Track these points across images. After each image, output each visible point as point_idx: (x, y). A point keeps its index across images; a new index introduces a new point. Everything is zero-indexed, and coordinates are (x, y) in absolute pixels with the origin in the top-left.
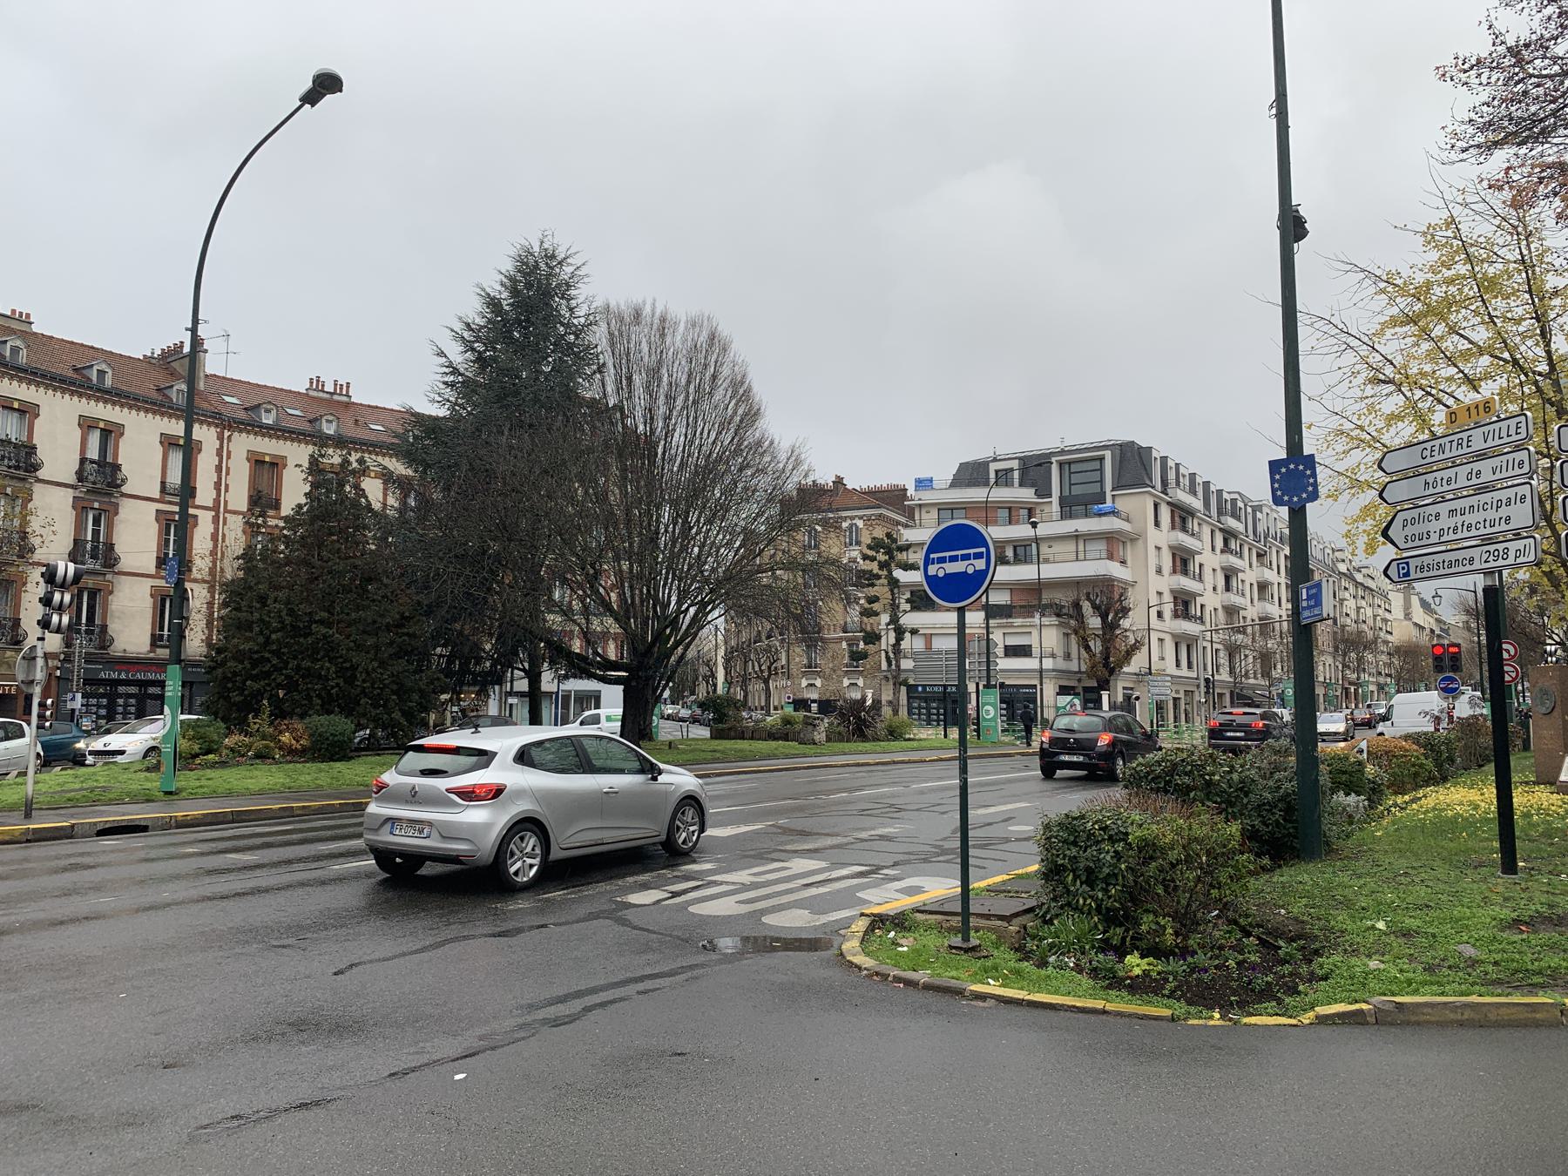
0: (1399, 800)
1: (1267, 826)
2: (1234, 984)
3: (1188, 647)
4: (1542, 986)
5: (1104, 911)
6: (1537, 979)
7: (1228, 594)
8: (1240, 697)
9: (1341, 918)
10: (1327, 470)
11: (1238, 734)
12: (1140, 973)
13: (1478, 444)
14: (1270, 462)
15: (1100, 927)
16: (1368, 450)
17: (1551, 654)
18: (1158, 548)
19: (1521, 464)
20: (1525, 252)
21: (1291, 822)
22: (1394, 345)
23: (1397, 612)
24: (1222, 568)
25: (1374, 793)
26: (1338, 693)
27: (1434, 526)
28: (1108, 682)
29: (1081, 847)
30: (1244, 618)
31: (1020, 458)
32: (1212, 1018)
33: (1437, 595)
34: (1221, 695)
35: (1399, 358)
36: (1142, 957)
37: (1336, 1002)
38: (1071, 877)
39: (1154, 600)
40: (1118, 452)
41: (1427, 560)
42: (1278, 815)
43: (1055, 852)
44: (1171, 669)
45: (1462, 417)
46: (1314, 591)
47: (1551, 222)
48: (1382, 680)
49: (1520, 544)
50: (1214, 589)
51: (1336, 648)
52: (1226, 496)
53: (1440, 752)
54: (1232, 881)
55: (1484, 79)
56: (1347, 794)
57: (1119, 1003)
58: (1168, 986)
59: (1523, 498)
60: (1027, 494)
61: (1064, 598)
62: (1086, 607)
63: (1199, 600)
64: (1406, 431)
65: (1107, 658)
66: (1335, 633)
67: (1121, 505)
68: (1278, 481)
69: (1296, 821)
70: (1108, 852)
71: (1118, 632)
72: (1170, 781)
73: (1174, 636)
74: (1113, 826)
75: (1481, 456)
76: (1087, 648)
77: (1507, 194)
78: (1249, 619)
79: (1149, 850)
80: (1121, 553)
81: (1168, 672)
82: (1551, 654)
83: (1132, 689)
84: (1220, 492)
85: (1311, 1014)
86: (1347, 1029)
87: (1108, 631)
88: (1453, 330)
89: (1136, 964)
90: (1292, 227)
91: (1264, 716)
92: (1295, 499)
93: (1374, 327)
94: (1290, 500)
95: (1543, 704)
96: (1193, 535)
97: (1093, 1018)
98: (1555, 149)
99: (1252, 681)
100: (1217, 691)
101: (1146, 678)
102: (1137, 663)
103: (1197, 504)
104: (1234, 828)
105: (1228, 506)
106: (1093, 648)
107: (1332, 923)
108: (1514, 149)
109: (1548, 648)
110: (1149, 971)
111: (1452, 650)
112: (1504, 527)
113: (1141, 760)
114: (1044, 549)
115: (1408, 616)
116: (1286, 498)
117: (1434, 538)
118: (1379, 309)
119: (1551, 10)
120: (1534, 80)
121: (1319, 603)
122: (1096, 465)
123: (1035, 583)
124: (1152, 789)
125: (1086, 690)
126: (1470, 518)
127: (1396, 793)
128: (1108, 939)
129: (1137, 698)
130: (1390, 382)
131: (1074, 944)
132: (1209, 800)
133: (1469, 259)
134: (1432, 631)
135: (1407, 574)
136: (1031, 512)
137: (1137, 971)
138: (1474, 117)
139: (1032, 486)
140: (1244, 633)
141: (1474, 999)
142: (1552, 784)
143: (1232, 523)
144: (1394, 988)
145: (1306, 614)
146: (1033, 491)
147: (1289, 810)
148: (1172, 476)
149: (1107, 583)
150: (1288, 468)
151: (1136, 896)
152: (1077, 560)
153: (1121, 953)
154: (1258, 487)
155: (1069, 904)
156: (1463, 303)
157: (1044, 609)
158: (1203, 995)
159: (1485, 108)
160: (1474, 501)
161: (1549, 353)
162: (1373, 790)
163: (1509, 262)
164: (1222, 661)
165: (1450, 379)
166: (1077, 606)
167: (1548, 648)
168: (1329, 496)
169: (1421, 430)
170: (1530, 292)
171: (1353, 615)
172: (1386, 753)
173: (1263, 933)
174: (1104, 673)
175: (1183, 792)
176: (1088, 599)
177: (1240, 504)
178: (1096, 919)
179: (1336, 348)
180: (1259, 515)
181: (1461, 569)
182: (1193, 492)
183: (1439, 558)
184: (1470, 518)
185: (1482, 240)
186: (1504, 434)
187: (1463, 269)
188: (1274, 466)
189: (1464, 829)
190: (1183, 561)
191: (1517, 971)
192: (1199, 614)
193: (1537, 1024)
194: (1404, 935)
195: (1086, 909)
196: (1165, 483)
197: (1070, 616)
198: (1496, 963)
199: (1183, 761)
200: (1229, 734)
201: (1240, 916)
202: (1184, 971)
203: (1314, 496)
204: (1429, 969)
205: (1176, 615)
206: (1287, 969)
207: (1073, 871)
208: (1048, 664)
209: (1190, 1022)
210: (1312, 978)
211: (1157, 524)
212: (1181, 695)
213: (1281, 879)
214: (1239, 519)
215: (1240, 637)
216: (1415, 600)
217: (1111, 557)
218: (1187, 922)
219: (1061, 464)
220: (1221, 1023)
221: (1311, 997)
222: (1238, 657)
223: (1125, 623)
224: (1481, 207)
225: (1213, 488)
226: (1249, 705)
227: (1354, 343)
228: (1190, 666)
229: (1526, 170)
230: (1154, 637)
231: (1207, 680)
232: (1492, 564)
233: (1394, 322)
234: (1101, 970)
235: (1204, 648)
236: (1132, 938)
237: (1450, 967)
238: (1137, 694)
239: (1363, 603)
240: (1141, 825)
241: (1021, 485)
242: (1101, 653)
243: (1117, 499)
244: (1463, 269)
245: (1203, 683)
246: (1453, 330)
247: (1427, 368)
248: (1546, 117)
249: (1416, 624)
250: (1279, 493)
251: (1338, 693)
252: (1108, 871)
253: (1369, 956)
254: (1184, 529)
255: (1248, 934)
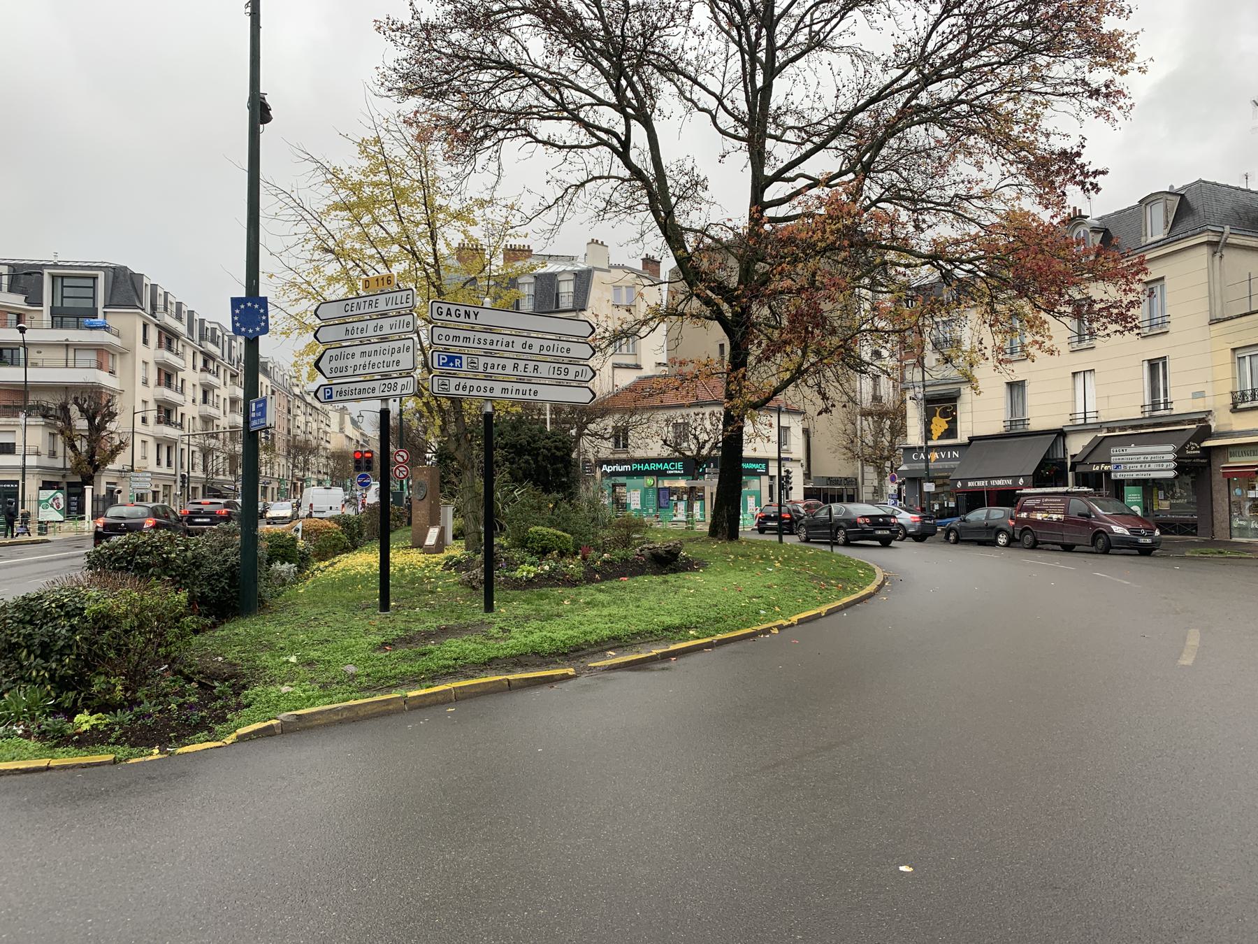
0: (322, 565)
1: (215, 592)
2: (173, 723)
3: (169, 448)
4: (395, 686)
5: (57, 679)
6: (393, 682)
7: (205, 406)
8: (211, 489)
9: (265, 658)
10: (282, 312)
11: (205, 520)
12: (88, 728)
13: (382, 306)
14: (233, 299)
15: (53, 694)
16: (313, 301)
17: (429, 460)
18: (145, 363)
19: (408, 324)
20: (424, 176)
21: (234, 587)
22: (337, 223)
23: (335, 427)
24: (201, 384)
25: (303, 561)
26: (289, 487)
27: (351, 362)
28: (92, 477)
29: (37, 625)
30: (217, 426)
31: (9, 265)
32: (151, 754)
33: (360, 416)
34: (195, 489)
35: (338, 235)
36: (91, 714)
37: (254, 722)
38: (24, 653)
39: (139, 407)
40: (111, 274)
41: (345, 387)
42: (224, 582)
43: (9, 632)
44: (153, 467)
45: (373, 284)
46: (261, 405)
47: (440, 158)
48: (321, 477)
49: (404, 381)
50: (194, 401)
51: (289, 453)
52: (207, 324)
53: (353, 529)
54: (178, 639)
55: (406, 43)
56: (282, 563)
57: (63, 758)
58: (114, 735)
59: (408, 348)
60: (17, 301)
61: (51, 401)
62: (74, 410)
63: (180, 410)
64: (340, 291)
65: (93, 456)
66: (289, 441)
67: (112, 321)
68: (237, 315)
69: (238, 586)
70: (63, 627)
71: (104, 433)
72: (132, 560)
73: (156, 438)
74: (70, 603)
75: (384, 315)
76: (73, 447)
77: (415, 130)
78: (221, 426)
79: (103, 620)
80: (111, 364)
81: (149, 469)
82: (429, 460)
83: (115, 484)
84: (202, 321)
85: (234, 736)
86: (260, 742)
87: (94, 432)
88: (376, 221)
89: (85, 721)
90: (260, 112)
91: (226, 506)
92: (251, 331)
93: (322, 208)
94: (246, 332)
95: (419, 493)
96: (177, 354)
97: (36, 776)
98: (446, 108)
99: (221, 477)
100: (192, 485)
101: (129, 474)
102: (121, 461)
103: (182, 328)
104: (183, 596)
105: (207, 334)
106: (79, 447)
107: (258, 662)
108: (422, 100)
109: (427, 455)
110: (97, 725)
111: (368, 455)
112: (396, 368)
113: (105, 544)
114: (32, 354)
115: (342, 430)
116: (243, 329)
117: (350, 372)
118: (326, 195)
119: (449, 7)
120: (435, 53)
121: (264, 416)
122: (90, 282)
123: (20, 386)
124: (114, 568)
125: (70, 485)
126: (374, 359)
127: (320, 560)
128: (60, 703)
129: (119, 492)
130: (332, 251)
131: (24, 712)
132: (165, 574)
133: (388, 171)
134: (358, 442)
135: (330, 397)
136: (20, 318)
137: (86, 727)
138: (398, 67)
139: (23, 293)
140: (217, 438)
141: (352, 702)
142: (421, 547)
143: (211, 347)
144: (298, 704)
145: (254, 423)
146: (23, 298)
147: (233, 578)
148: (160, 302)
149: (95, 390)
150: (246, 306)
151: (91, 661)
152: (67, 367)
153: (71, 713)
154: (223, 317)
155: (22, 678)
156: (383, 203)
157: (30, 411)
158: (142, 737)
159: (405, 63)
160: (377, 347)
161: (434, 250)
162: (302, 559)
163: (414, 180)
164: (197, 461)
165: (371, 257)
166: (64, 408)
167: (427, 455)
168: (282, 333)
169: (350, 291)
170: (425, 205)
171: (303, 428)
172: (316, 530)
173: (203, 678)
174: (86, 468)
175: (142, 569)
176: (76, 402)
177: (219, 333)
178: (49, 687)
179: (293, 218)
180: (234, 343)
181: (367, 395)
182: (179, 317)
183: (353, 386)
184: (374, 359)
185: (397, 159)
186: (398, 302)
187: (383, 177)
188: (235, 302)
189: (360, 582)
190: (167, 375)
191: (380, 678)
192: (179, 421)
193: (388, 713)
194: (309, 664)
195: (39, 680)
196: (154, 307)
197: (57, 418)
198: (368, 675)
199: (144, 543)
200: (197, 520)
201: (185, 667)
202: (130, 719)
203: (265, 330)
204: (324, 686)
205: (159, 422)
206: (220, 703)
207: (27, 647)
208: (31, 461)
209: (131, 761)
210: (240, 706)
211: (145, 342)
212: (161, 489)
213: (222, 633)
214: (217, 345)
215: (213, 441)
216: (347, 418)
217: (100, 367)
218: (136, 679)
219: (53, 277)
220: (160, 756)
221: (237, 721)
222: (210, 457)
223: (111, 426)
224: (398, 135)
225: (196, 317)
226: (218, 497)
227: (308, 217)
228: (169, 464)
229: (428, 117)
230: (138, 439)
231: (183, 476)
232: (386, 393)
233: (336, 207)
234: (50, 732)
235: (182, 450)
236: (83, 700)
237: (338, 683)
238: (119, 488)
239: (311, 419)
240: (97, 601)
241: (10, 291)
242: (86, 451)
243: (108, 316)
244: (383, 177)
245: (179, 479)
246: (376, 221)
247: (357, 246)
248: (442, 83)
249: (347, 436)
250: (238, 325)
251: (289, 487)
252: (62, 643)
253: (282, 684)
254: (169, 349)
255: (190, 680)
